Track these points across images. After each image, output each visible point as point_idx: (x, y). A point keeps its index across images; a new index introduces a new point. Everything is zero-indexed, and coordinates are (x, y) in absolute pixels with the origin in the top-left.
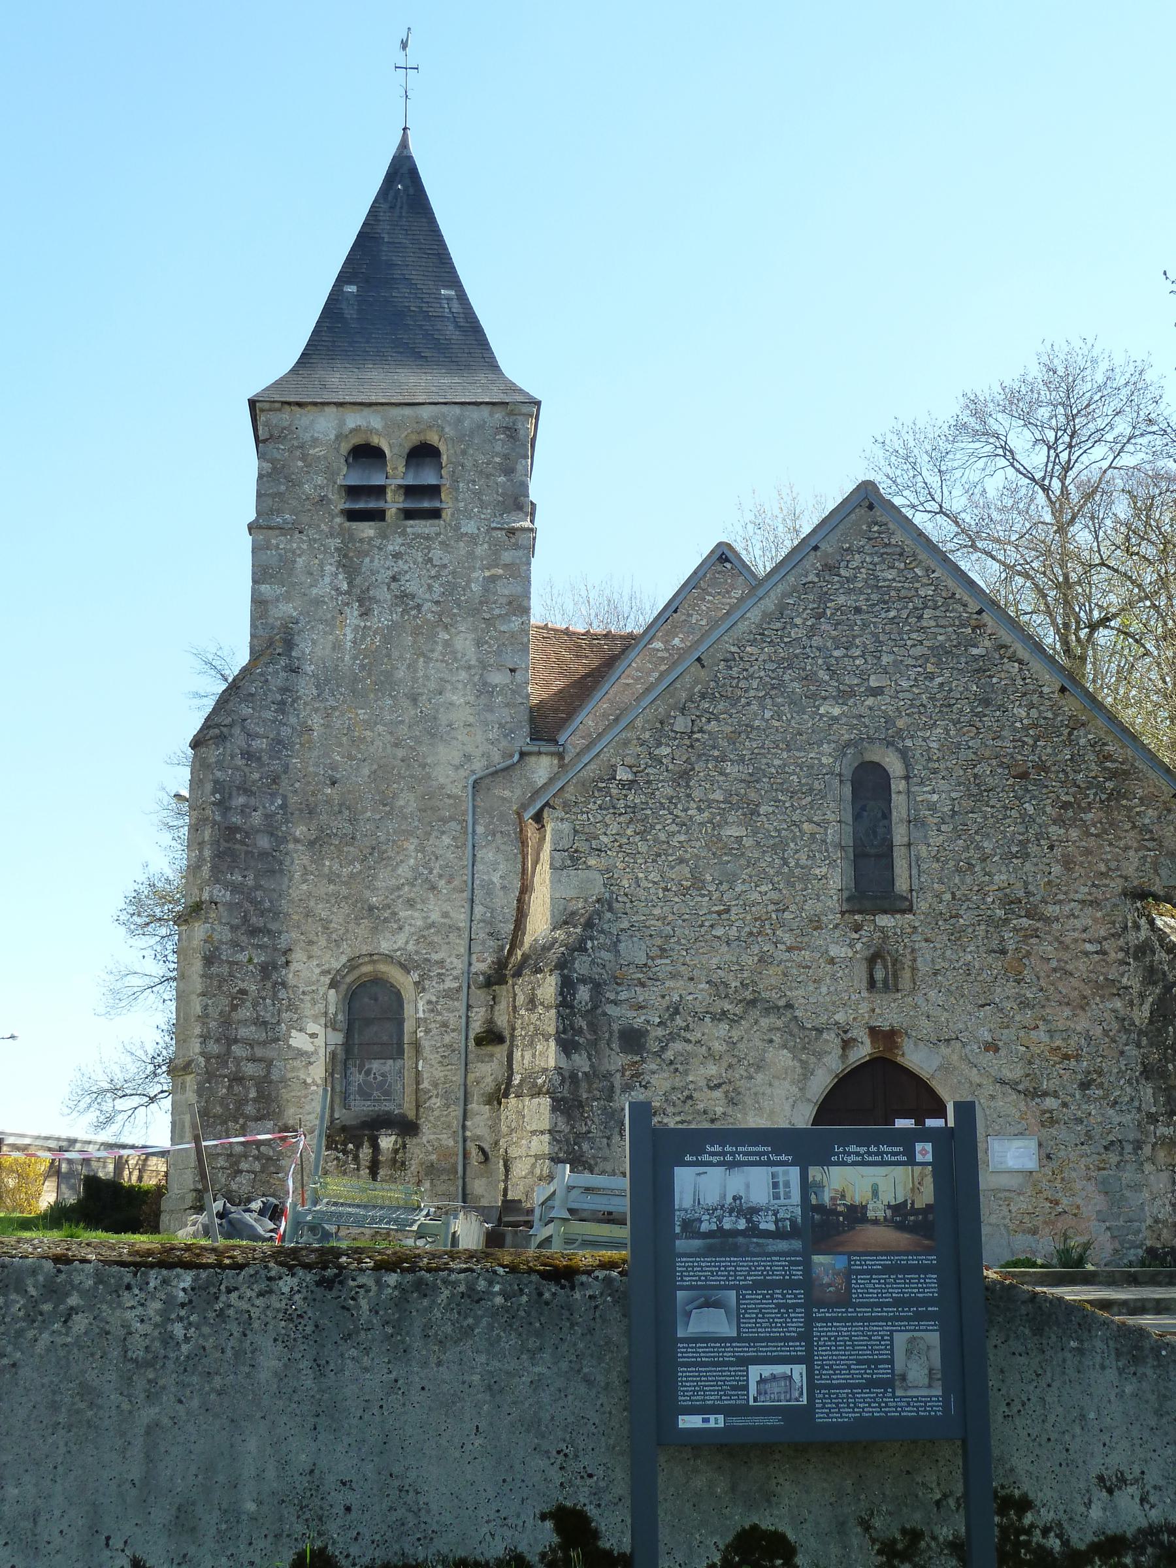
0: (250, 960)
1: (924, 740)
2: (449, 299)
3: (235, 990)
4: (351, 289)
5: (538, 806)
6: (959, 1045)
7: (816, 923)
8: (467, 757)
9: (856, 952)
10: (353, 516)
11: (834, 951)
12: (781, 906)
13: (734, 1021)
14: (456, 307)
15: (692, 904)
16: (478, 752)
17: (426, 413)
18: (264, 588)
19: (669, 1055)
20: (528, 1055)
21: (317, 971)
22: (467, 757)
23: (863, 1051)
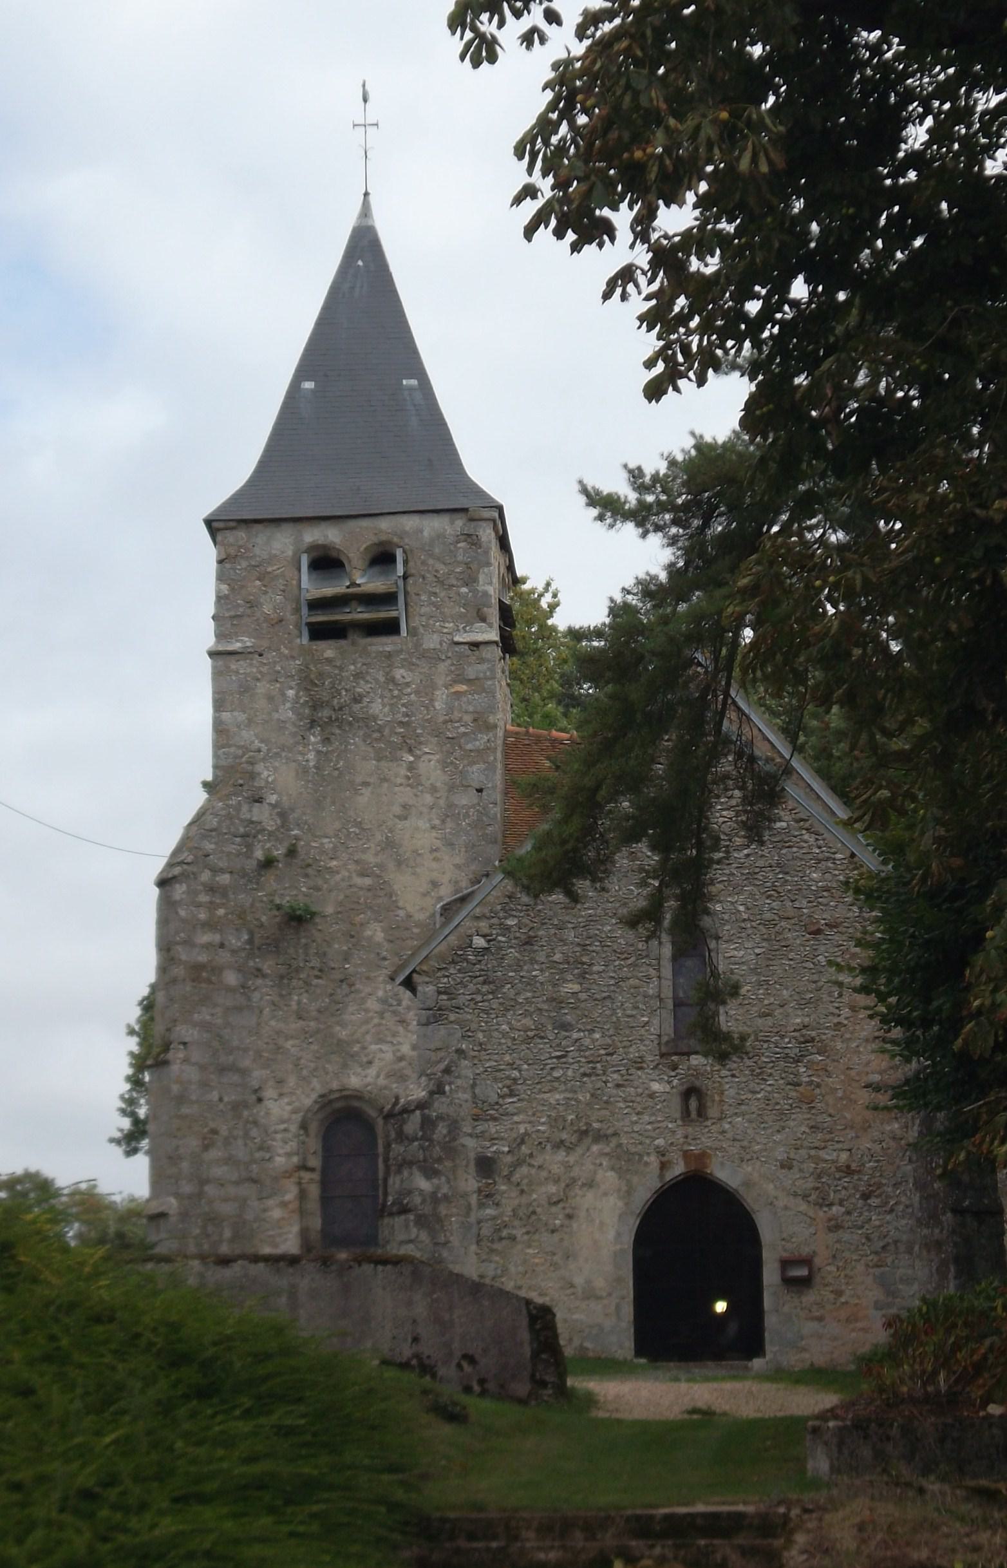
0: (221, 1100)
1: (732, 903)
2: (411, 389)
3: (206, 1130)
4: (308, 385)
5: (407, 973)
6: (759, 1163)
7: (639, 1063)
8: (435, 884)
9: (673, 1087)
10: (319, 632)
11: (656, 1086)
12: (610, 1050)
13: (570, 1149)
14: (418, 397)
15: (535, 1051)
16: (445, 879)
17: (384, 524)
18: (226, 716)
19: (516, 1177)
20: (398, 1179)
21: (289, 1108)
22: (435, 884)
23: (678, 1169)
